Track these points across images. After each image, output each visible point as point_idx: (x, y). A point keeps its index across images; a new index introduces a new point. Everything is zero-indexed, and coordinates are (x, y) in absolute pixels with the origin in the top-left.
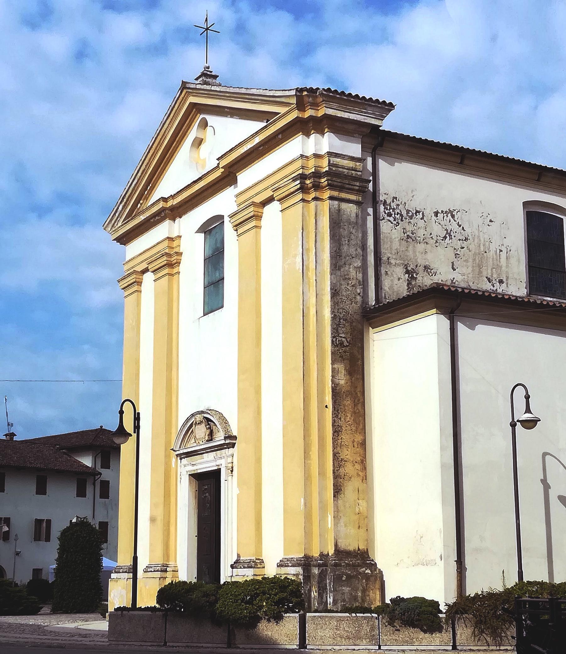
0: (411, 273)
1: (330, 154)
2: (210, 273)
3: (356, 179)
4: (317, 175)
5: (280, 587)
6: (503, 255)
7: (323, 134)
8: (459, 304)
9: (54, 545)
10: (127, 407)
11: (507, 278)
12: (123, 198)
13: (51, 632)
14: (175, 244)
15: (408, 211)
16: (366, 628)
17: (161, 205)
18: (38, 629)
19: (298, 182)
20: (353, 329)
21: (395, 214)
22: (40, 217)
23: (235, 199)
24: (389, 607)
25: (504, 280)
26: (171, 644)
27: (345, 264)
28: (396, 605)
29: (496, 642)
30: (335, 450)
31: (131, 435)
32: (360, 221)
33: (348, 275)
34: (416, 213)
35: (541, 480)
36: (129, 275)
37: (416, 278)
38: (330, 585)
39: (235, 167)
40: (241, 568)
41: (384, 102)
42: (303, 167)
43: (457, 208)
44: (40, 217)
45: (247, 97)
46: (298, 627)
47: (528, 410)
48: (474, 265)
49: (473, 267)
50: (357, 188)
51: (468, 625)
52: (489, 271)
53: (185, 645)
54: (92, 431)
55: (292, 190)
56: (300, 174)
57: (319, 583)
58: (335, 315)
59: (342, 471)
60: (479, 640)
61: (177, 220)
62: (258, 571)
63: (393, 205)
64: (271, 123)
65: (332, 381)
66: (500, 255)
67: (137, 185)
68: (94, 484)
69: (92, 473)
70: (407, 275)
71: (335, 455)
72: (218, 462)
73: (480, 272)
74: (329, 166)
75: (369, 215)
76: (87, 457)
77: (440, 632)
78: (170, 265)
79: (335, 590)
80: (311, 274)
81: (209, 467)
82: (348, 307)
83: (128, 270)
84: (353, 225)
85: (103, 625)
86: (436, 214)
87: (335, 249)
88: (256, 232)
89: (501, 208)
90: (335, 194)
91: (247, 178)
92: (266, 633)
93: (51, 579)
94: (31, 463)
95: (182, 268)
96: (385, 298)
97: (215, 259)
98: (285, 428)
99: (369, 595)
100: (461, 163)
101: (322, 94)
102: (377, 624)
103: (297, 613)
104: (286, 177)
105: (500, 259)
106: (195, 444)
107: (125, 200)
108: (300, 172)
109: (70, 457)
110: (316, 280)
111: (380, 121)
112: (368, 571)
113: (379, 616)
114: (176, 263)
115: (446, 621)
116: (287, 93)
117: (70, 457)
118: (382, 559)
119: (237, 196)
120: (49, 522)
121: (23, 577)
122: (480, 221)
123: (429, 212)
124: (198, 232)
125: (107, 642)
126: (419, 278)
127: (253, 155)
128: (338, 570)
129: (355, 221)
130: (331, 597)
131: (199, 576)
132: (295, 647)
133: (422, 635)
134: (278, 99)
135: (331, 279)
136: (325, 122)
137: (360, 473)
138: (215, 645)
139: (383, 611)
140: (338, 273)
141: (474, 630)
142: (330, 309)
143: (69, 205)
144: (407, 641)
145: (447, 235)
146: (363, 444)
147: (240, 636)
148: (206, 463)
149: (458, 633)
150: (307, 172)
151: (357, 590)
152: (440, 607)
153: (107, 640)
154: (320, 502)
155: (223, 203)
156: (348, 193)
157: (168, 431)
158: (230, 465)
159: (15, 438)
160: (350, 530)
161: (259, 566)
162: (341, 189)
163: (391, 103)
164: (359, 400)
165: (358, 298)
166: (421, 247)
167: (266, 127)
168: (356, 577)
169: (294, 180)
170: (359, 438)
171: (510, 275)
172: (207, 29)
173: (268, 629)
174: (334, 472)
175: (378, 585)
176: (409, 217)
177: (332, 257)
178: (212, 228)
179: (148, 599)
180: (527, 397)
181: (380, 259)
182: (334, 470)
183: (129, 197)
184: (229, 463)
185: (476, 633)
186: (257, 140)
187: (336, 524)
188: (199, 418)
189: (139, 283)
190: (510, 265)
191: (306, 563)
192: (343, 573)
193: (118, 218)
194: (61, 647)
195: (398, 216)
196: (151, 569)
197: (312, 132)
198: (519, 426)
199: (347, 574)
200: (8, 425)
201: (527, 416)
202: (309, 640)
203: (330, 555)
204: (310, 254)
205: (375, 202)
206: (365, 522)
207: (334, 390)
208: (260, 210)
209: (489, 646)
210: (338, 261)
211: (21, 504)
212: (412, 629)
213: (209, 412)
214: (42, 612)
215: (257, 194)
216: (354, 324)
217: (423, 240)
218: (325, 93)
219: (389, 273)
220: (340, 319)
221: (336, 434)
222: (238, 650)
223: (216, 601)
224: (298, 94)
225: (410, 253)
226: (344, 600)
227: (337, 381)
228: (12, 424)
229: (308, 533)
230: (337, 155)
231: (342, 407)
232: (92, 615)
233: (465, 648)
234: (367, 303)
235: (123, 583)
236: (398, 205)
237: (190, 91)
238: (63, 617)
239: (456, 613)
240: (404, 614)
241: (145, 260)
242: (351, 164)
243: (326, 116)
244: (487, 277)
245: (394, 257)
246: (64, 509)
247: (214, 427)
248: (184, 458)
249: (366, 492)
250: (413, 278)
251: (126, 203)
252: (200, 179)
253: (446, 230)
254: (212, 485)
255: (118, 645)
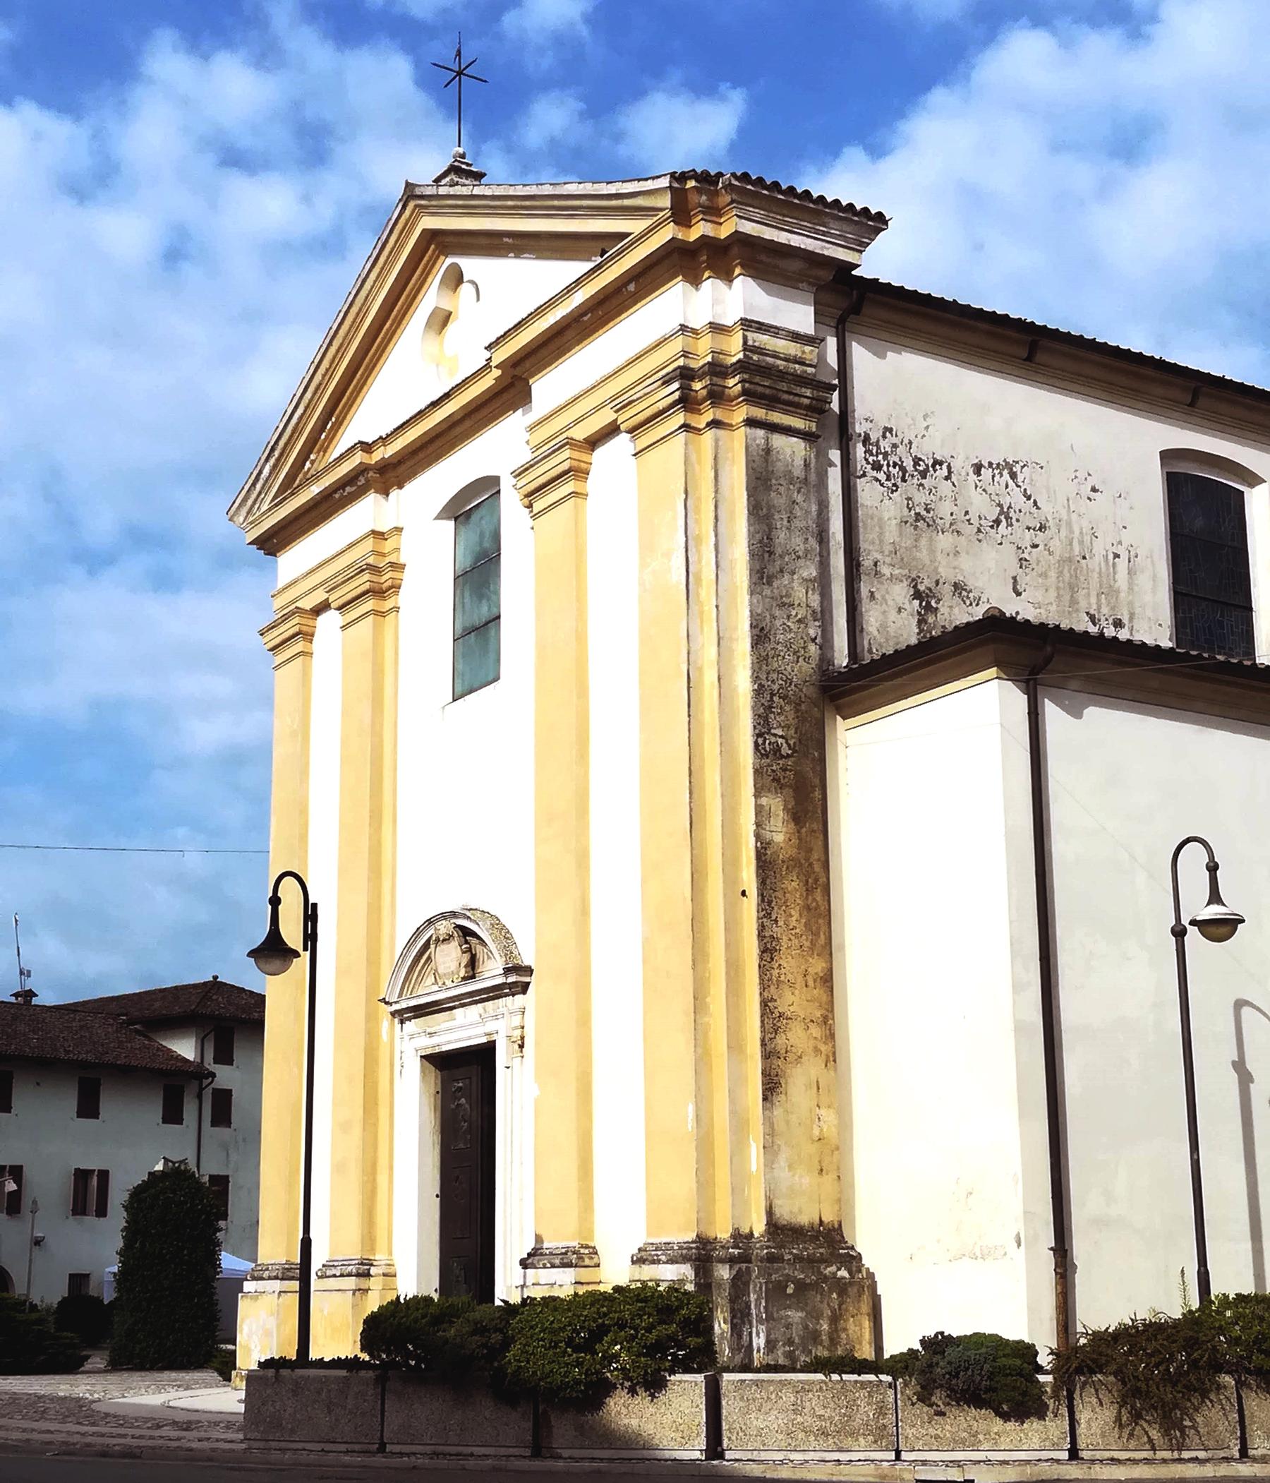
0: (925, 599)
1: (748, 324)
2: (468, 606)
3: (804, 381)
4: (717, 369)
5: (659, 1311)
6: (1122, 564)
7: (728, 278)
8: (1049, 660)
9: (117, 1217)
10: (289, 890)
11: (1132, 617)
12: (273, 449)
13: (107, 1415)
14: (388, 546)
15: (917, 461)
16: (865, 1410)
17: (358, 458)
18: (78, 1409)
19: (676, 385)
20: (801, 717)
21: (888, 465)
22: (92, 572)
23: (527, 436)
24: (917, 1358)
25: (1125, 621)
26: (397, 1448)
27: (781, 571)
28: (935, 1353)
29: (1171, 1440)
30: (766, 994)
31: (297, 954)
32: (813, 477)
33: (788, 596)
34: (933, 466)
35: (1234, 1063)
36: (285, 618)
37: (937, 609)
38: (758, 1306)
39: (527, 364)
40: (544, 1267)
41: (866, 210)
42: (685, 354)
43: (1022, 456)
44: (92, 572)
45: (556, 203)
46: (703, 1407)
47: (1215, 898)
48: (1061, 585)
49: (1058, 588)
50: (806, 401)
51: (1105, 1400)
52: (1093, 600)
53: (428, 1449)
54: (195, 986)
55: (661, 405)
56: (679, 367)
57: (733, 1300)
58: (761, 686)
59: (781, 1041)
60: (1131, 1435)
61: (395, 493)
62: (585, 1275)
63: (885, 445)
64: (611, 258)
65: (758, 836)
66: (1114, 564)
67: (304, 419)
68: (200, 1097)
69: (197, 1074)
70: (916, 602)
71: (765, 1004)
72: (490, 1026)
73: (1073, 602)
74: (745, 350)
75: (832, 464)
76: (183, 1045)
77: (1042, 1417)
78: (378, 592)
79: (770, 1318)
80: (706, 593)
81: (470, 1038)
82: (789, 668)
83: (283, 608)
84: (798, 485)
85: (226, 1399)
86: (978, 468)
87: (758, 536)
88: (576, 507)
89: (1112, 464)
90: (759, 413)
91: (550, 388)
92: (626, 1421)
93: (109, 1296)
94: (67, 1052)
95: (403, 598)
96: (870, 651)
97: (479, 574)
98: (646, 942)
99: (845, 1330)
100: (1029, 359)
101: (729, 187)
102: (891, 1400)
103: (699, 1371)
104: (646, 377)
105: (1115, 573)
106: (436, 988)
107: (277, 453)
108: (681, 362)
109: (150, 1039)
110: (717, 607)
111: (857, 254)
112: (843, 1273)
113: (895, 1379)
114: (391, 588)
115: (1053, 1391)
116: (650, 185)
117: (150, 1039)
118: (871, 1242)
119: (531, 428)
120: (104, 1175)
121: (45, 1289)
122: (1071, 489)
123: (962, 465)
124: (439, 517)
125: (242, 1442)
126: (943, 609)
127: (570, 334)
128: (777, 1271)
129: (802, 476)
130: (762, 1335)
131: (444, 1288)
132: (697, 1455)
133: (998, 1425)
134: (627, 202)
135: (751, 604)
136: (735, 250)
137: (823, 1048)
138: (503, 1451)
139: (906, 1367)
140: (767, 592)
141: (1119, 1412)
142: (749, 673)
143: (152, 551)
144: (963, 1441)
145: (1002, 517)
146: (827, 980)
147: (562, 1429)
148: (460, 1030)
149: (1083, 1416)
150: (695, 365)
151: (818, 1316)
152: (1038, 1359)
153: (241, 1436)
154: (733, 1112)
155: (500, 449)
156: (786, 412)
157: (373, 959)
158: (518, 1033)
159: (35, 1001)
160: (801, 1177)
161: (587, 1262)
162: (771, 402)
163: (880, 215)
164: (816, 880)
165: (813, 648)
166: (945, 541)
167: (599, 267)
168: (815, 1286)
169: (667, 382)
170: (818, 966)
171: (1137, 610)
172: (460, 73)
173: (629, 1412)
174: (763, 1044)
175: (865, 1307)
176: (920, 472)
177: (752, 555)
178: (472, 507)
179: (337, 1337)
180: (1213, 868)
181: (859, 565)
182: (763, 1040)
183: (286, 444)
184: (516, 1028)
185: (1124, 1419)
186: (579, 298)
187: (769, 1164)
188: (444, 927)
189: (308, 636)
190: (1136, 589)
191: (701, 1254)
192: (788, 1279)
193: (260, 493)
194: (129, 1454)
195: (894, 471)
196: (334, 1271)
197: (706, 274)
198: (1193, 933)
199: (787, 1282)
200: (22, 973)
201: (1214, 911)
202: (730, 1439)
203: (756, 1235)
204: (704, 548)
205: (845, 437)
206: (833, 1159)
207: (760, 855)
208: (584, 457)
209: (1154, 1449)
210: (766, 563)
211: (46, 1137)
212: (973, 1412)
213: (468, 914)
214: (87, 1367)
215: (577, 422)
216: (803, 707)
217: (951, 524)
218: (736, 183)
219: (877, 595)
220: (772, 695)
221: (767, 956)
222: (561, 1464)
223: (506, 1344)
224: (676, 185)
225: (923, 555)
226: (790, 1342)
227: (768, 835)
228: (29, 972)
229: (705, 1183)
230: (762, 327)
231: (779, 894)
232: (197, 1375)
233: (1098, 1455)
234: (830, 662)
235: (270, 1301)
236: (895, 446)
237: (423, 202)
238: (136, 1377)
239: (1079, 1371)
240: (958, 1373)
241: (321, 584)
242: (792, 349)
243: (738, 237)
244: (1087, 613)
245: (888, 560)
246: (136, 1145)
247: (479, 948)
248: (409, 1019)
249: (834, 1091)
250: (929, 608)
251: (278, 460)
252: (447, 396)
253: (1000, 505)
254: (474, 1079)
255: (269, 1449)
